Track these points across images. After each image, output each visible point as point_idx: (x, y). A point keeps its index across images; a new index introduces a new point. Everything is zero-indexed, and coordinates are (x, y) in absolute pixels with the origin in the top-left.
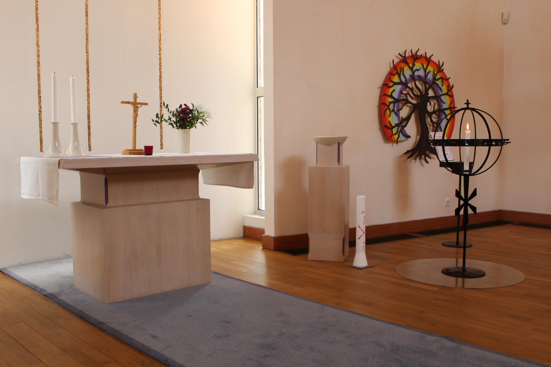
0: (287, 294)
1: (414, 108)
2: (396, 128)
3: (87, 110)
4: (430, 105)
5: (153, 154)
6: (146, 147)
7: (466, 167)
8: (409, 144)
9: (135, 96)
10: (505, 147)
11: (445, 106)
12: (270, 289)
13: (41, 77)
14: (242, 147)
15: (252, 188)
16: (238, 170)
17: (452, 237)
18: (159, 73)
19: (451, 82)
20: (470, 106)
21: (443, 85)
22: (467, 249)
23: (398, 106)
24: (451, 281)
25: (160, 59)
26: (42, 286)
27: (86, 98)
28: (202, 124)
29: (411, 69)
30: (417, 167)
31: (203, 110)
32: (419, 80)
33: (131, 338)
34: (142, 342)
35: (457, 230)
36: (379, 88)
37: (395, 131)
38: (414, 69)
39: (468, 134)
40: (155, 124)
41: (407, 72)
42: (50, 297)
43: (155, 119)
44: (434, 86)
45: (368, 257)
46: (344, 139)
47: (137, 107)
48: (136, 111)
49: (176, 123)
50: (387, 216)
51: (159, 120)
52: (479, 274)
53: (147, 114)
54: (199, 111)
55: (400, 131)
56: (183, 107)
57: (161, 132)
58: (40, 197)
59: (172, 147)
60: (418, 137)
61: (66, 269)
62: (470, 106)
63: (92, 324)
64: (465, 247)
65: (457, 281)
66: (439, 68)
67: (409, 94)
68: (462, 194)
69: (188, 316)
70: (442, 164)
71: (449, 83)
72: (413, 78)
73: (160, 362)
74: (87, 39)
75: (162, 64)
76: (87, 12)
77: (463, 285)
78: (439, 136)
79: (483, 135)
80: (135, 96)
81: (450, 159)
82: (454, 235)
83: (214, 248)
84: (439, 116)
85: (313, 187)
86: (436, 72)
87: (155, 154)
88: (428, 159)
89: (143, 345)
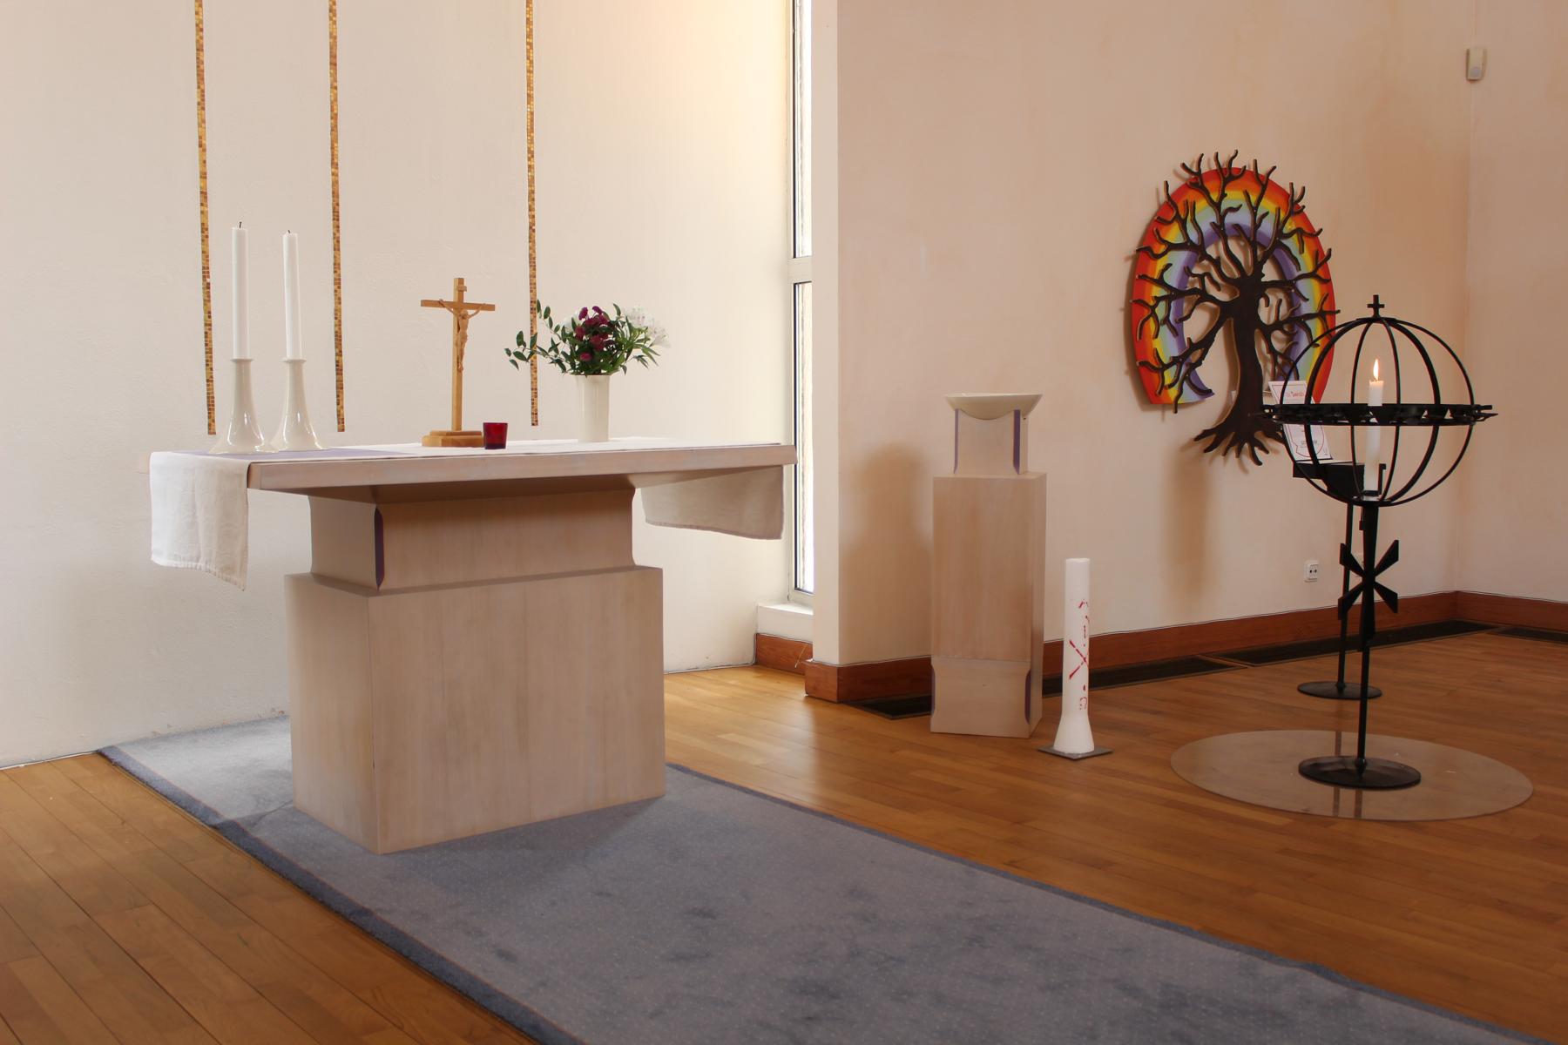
0: (871, 831)
1: (1224, 314)
2: (1174, 368)
3: (333, 322)
4: (1268, 304)
5: (508, 443)
6: (489, 427)
7: (1370, 483)
8: (1208, 413)
9: (460, 287)
10: (1478, 426)
11: (1306, 308)
12: (825, 815)
13: (211, 233)
14: (752, 424)
15: (778, 537)
16: (741, 490)
17: (1324, 668)
18: (527, 220)
19: (1325, 242)
20: (1383, 313)
21: (1302, 251)
22: (1370, 704)
23: (1179, 309)
24: (1320, 796)
25: (531, 181)
26: (208, 799)
27: (332, 287)
28: (643, 361)
29: (1216, 206)
30: (1229, 475)
31: (646, 323)
32: (1238, 238)
33: (442, 958)
34: (473, 971)
35: (1340, 646)
36: (1127, 259)
37: (1169, 376)
38: (1224, 206)
39: (1376, 392)
40: (513, 362)
41: (1205, 216)
42: (230, 833)
43: (514, 348)
44: (1278, 253)
45: (1096, 724)
46: (1032, 401)
47: (465, 317)
48: (460, 327)
49: (570, 358)
50: (1147, 608)
51: (525, 351)
52: (1402, 779)
53: (491, 336)
54: (635, 326)
55: (1185, 378)
56: (591, 314)
57: (534, 379)
58: (201, 564)
59: (561, 426)
60: (1234, 394)
61: (274, 750)
62: (1383, 313)
63: (338, 913)
64: (1364, 696)
65: (1337, 797)
66: (1292, 204)
67: (1209, 275)
68: (1358, 553)
69: (600, 894)
70: (1300, 470)
71: (1318, 244)
72: (1220, 230)
73: (519, 1030)
74: (334, 129)
75: (536, 196)
76: (333, 56)
77: (1358, 812)
78: (1296, 392)
79: (1418, 393)
80: (460, 287)
81: (1323, 455)
82: (1329, 663)
83: (673, 696)
84: (1292, 339)
85: (940, 525)
86: (1282, 216)
87: (514, 445)
88: (1259, 453)
89: (473, 979)
